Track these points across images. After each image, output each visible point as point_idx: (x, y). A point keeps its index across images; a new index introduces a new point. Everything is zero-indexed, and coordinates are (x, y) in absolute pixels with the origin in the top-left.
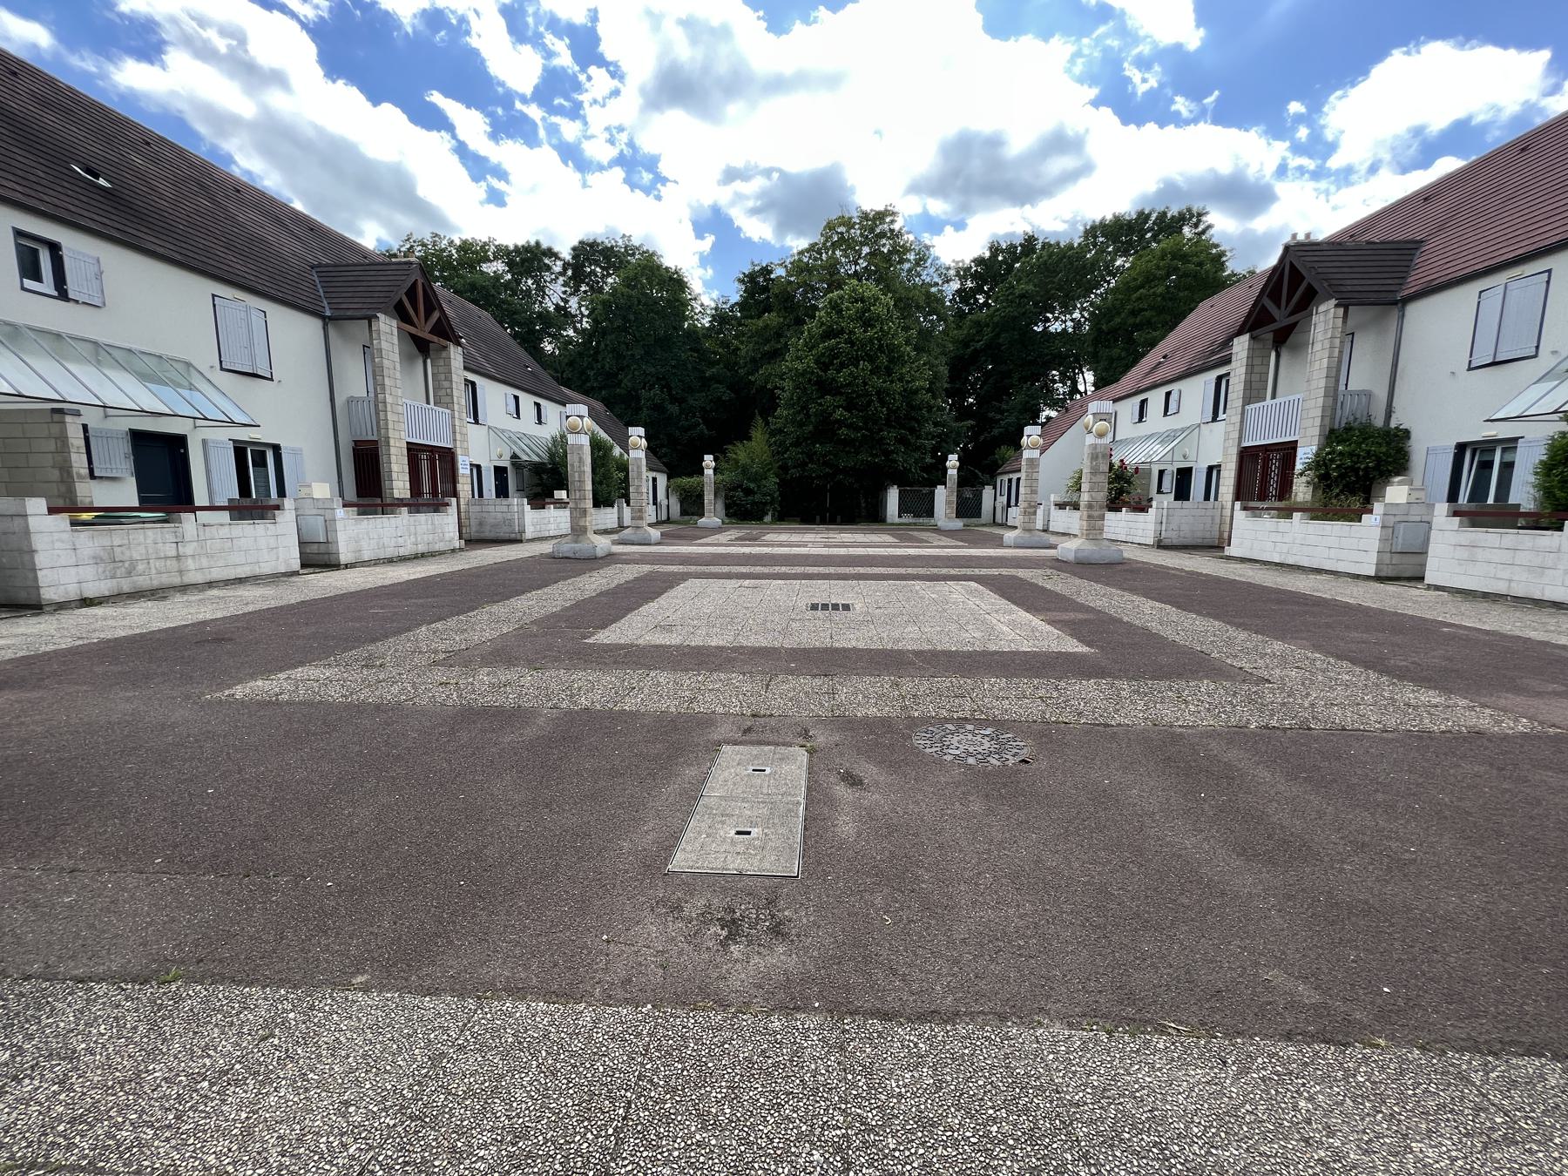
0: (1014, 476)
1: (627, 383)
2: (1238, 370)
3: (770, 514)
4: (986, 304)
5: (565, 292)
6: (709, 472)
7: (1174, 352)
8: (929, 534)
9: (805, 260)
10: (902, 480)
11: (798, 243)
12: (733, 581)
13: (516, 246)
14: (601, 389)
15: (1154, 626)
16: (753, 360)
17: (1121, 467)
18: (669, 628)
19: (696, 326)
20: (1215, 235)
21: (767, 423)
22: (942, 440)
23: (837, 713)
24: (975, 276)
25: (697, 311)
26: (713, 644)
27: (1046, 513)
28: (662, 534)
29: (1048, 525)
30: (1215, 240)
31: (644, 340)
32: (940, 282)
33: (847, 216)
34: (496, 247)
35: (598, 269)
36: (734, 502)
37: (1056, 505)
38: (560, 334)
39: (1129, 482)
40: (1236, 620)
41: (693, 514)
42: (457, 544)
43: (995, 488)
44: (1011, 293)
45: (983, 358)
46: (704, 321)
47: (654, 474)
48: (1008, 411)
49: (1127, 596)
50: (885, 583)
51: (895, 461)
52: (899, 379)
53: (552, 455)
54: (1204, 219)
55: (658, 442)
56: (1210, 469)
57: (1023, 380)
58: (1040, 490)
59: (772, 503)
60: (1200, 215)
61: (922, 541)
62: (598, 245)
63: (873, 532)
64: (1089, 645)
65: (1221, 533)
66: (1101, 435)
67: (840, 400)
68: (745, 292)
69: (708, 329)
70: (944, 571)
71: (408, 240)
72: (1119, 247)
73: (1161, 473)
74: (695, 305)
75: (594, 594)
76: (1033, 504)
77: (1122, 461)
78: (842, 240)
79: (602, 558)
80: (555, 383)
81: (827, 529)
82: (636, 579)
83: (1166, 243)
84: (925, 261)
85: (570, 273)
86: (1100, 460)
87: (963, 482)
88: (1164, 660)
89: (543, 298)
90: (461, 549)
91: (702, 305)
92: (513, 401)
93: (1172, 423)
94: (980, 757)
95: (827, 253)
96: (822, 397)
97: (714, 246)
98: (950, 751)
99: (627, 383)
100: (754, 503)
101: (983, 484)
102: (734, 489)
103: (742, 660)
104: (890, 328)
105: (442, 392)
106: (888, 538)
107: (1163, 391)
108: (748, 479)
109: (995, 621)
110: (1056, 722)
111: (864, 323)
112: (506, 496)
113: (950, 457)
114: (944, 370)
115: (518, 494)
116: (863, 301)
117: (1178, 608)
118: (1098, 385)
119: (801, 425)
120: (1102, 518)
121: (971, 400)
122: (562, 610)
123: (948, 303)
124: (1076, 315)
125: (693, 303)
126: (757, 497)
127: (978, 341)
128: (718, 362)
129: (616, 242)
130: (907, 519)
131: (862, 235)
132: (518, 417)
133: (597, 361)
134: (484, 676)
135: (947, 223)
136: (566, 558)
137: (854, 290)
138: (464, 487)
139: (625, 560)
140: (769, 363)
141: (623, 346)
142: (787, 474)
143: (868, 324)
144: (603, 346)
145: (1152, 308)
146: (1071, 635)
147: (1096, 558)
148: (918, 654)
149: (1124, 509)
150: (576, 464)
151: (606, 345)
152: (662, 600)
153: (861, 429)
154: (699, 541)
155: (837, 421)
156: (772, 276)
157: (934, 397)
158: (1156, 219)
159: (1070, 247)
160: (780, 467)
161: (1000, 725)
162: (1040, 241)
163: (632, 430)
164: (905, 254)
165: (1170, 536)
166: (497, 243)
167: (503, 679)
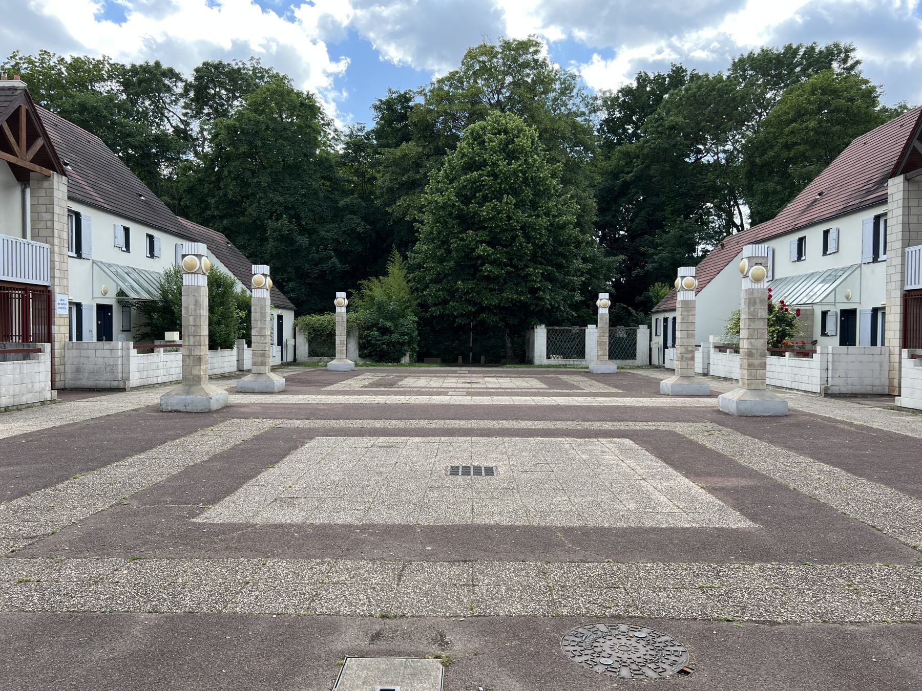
0: (670, 316)
1: (252, 211)
2: (895, 209)
3: (408, 354)
4: (635, 134)
5: (185, 115)
6: (341, 311)
7: (830, 189)
8: (579, 378)
9: (446, 88)
10: (550, 319)
11: (440, 70)
12: (365, 439)
13: (133, 66)
14: (222, 217)
15: (822, 495)
16: (391, 190)
17: (782, 309)
18: (290, 502)
19: (328, 153)
20: (863, 71)
21: (405, 258)
22: (592, 276)
23: (477, 611)
24: (623, 106)
25: (330, 137)
26: (340, 522)
27: (706, 355)
28: (287, 379)
29: (708, 368)
30: (863, 76)
31: (271, 167)
32: (587, 112)
33: (489, 45)
34: (111, 65)
35: (223, 92)
36: (368, 341)
37: (716, 347)
38: (179, 158)
39: (790, 325)
40: (909, 487)
41: (323, 355)
42: (48, 394)
43: (650, 327)
44: (661, 125)
45: (634, 190)
46: (338, 148)
47: (280, 312)
48: (661, 245)
49: (794, 456)
50: (532, 440)
51: (542, 299)
52: (545, 214)
53: (164, 292)
54: (852, 55)
55: (285, 276)
56: (875, 311)
57: (676, 212)
58: (697, 333)
59: (410, 343)
60: (848, 51)
61: (572, 387)
62: (224, 67)
63: (519, 375)
64: (753, 518)
65: (891, 380)
66: (757, 280)
67: (483, 235)
68: (381, 119)
69: (343, 156)
70: (596, 425)
71: (14, 57)
72: (768, 81)
73: (824, 314)
74: (328, 131)
75: (206, 458)
76: (690, 348)
77: (782, 302)
78: (484, 69)
79: (217, 411)
80: (172, 214)
81: (470, 372)
82: (256, 438)
83: (815, 78)
84: (571, 91)
85: (192, 94)
86: (758, 306)
87: (615, 320)
88: (833, 537)
89: (162, 120)
90: (52, 401)
91: (336, 130)
92: (121, 234)
93: (830, 263)
94: (634, 667)
95: (468, 82)
96: (464, 231)
97: (349, 69)
98: (602, 660)
99: (252, 211)
100: (390, 343)
101: (639, 322)
102: (369, 328)
103: (372, 543)
104: (535, 160)
105: (41, 225)
106: (534, 383)
107: (821, 229)
108: (385, 317)
109: (651, 489)
110: (718, 620)
111: (508, 155)
112: (110, 339)
113: (601, 295)
114: (592, 203)
115: (123, 335)
116: (506, 132)
117: (848, 471)
118: (758, 218)
119: (442, 260)
120: (764, 366)
121: (622, 232)
122: (168, 480)
123: (596, 133)
124: (729, 147)
125: (326, 129)
126: (395, 337)
127: (628, 173)
128: (352, 192)
129: (244, 64)
130: (556, 360)
131: (504, 64)
132: (128, 250)
133: (220, 189)
134: (71, 570)
135: (594, 50)
136: (176, 411)
137: (497, 122)
138: (60, 329)
139: (244, 413)
140: (407, 194)
141: (248, 174)
142: (427, 311)
143: (511, 156)
144: (226, 173)
145: (805, 142)
146: (734, 507)
147: (758, 410)
148: (568, 531)
149: (787, 354)
150: (192, 307)
151: (230, 172)
152: (285, 465)
153: (506, 265)
154: (329, 388)
155: (480, 257)
156: (411, 104)
157: (583, 232)
158: (804, 54)
159: (719, 79)
160: (420, 305)
161: (655, 623)
162: (689, 73)
163: (256, 268)
164: (551, 84)
165: (839, 385)
166: (112, 62)
167: (94, 573)
